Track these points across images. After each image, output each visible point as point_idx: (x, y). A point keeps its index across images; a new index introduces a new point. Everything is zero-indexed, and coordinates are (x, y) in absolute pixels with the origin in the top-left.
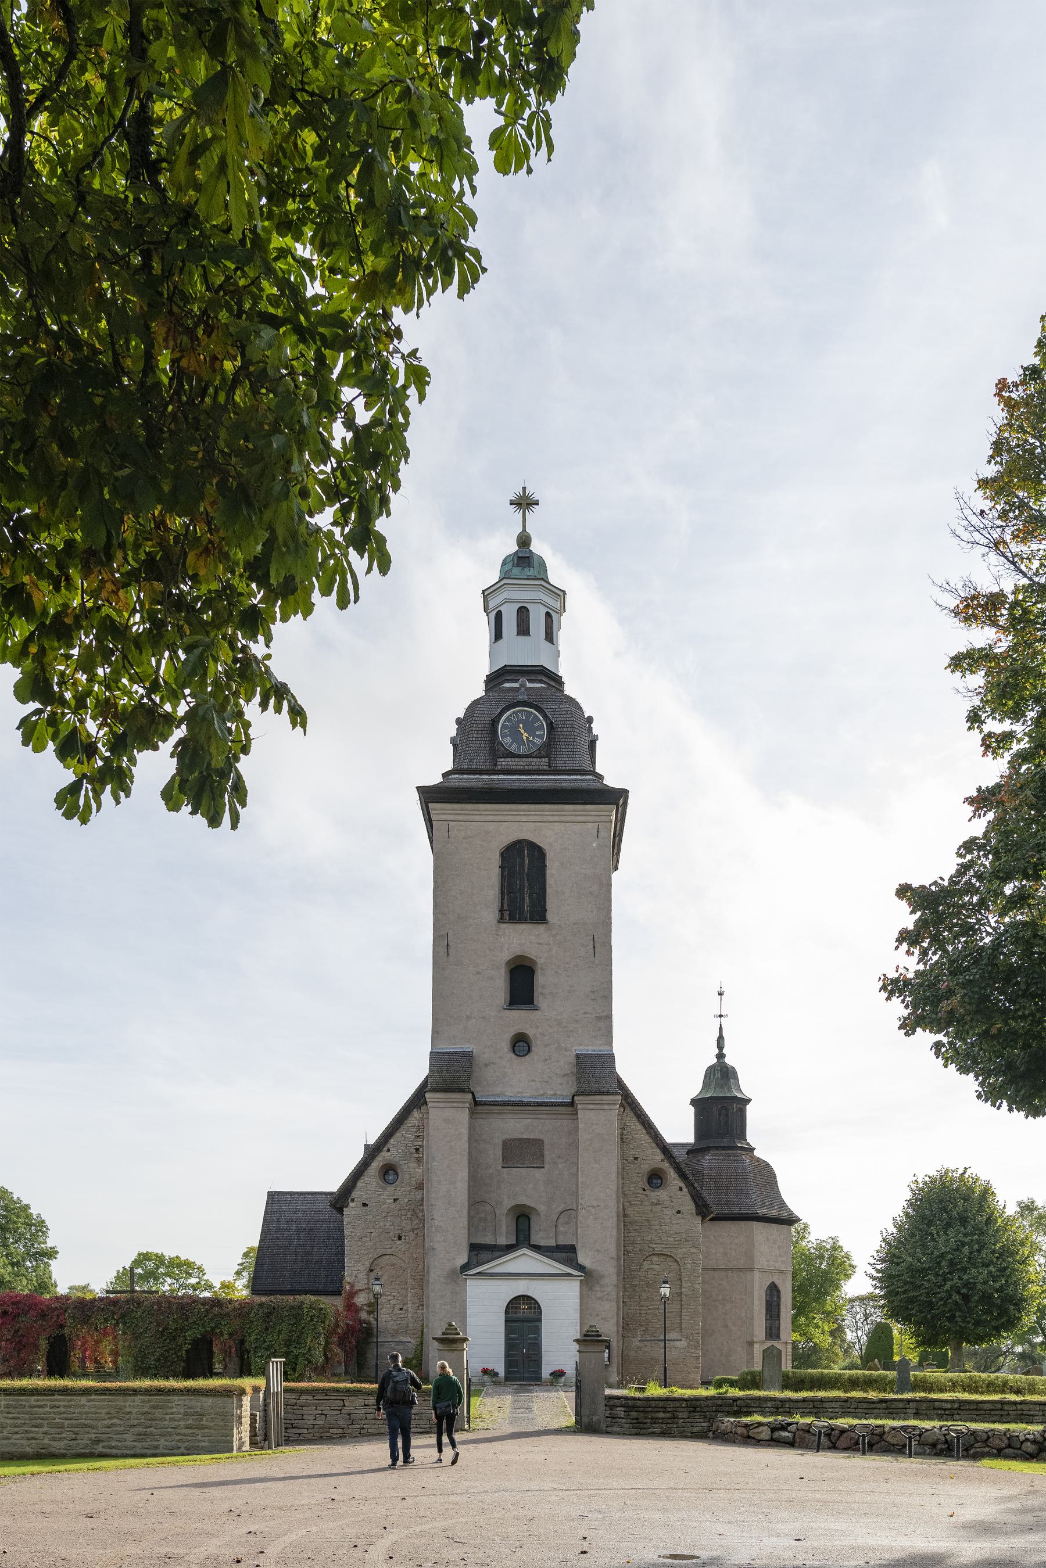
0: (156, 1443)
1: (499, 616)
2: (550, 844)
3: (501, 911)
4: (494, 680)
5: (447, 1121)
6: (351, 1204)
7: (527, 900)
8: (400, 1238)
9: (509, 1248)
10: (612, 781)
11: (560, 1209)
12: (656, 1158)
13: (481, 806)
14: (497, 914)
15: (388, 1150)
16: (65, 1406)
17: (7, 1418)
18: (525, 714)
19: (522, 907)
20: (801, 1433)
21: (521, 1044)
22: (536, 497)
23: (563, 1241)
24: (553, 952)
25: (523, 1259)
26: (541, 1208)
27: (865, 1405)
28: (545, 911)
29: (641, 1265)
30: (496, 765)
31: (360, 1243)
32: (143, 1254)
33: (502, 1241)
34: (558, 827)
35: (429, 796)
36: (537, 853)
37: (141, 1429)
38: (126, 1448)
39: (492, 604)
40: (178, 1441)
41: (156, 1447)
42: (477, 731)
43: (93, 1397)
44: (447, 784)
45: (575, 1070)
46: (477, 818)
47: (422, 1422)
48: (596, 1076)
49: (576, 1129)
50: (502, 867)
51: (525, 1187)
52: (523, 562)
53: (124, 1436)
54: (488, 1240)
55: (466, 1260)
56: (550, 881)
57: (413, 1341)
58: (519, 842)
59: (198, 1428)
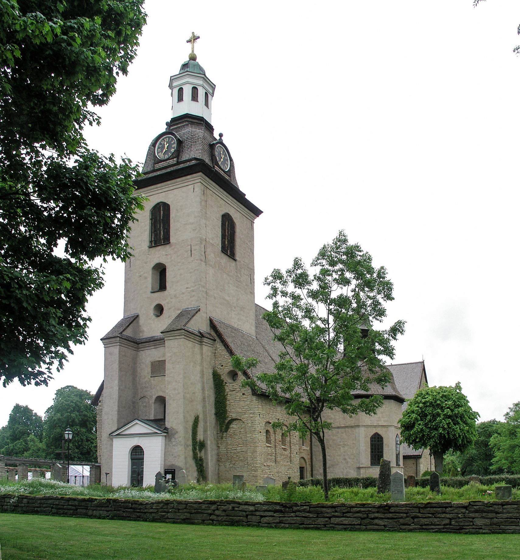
1: (181, 91)
3: (151, 242)
21: (159, 310)
24: (173, 258)
25: (137, 426)
52: (191, 66)
58: (158, 204)
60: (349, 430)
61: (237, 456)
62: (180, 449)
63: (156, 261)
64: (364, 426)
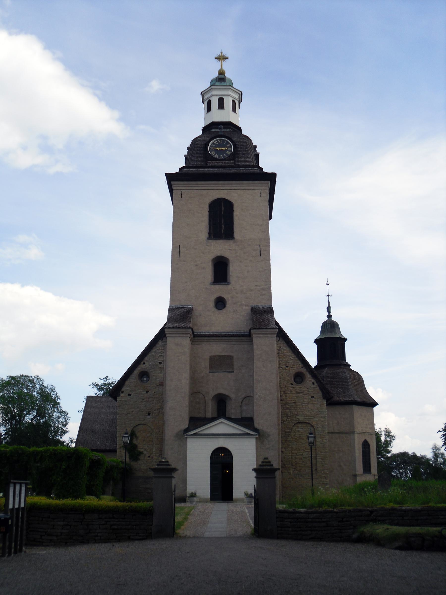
1: (209, 103)
4: (205, 129)
8: (149, 414)
10: (266, 170)
11: (243, 396)
13: (199, 182)
14: (207, 235)
15: (144, 363)
18: (222, 141)
21: (220, 303)
22: (227, 56)
23: (245, 415)
25: (221, 426)
26: (232, 396)
28: (233, 233)
29: (292, 429)
30: (207, 164)
31: (126, 417)
33: (209, 415)
35: (171, 178)
39: (205, 97)
46: (197, 188)
48: (263, 319)
49: (252, 349)
51: (222, 383)
52: (221, 79)
55: (187, 426)
61: (303, 462)
63: (218, 253)
64: (359, 433)
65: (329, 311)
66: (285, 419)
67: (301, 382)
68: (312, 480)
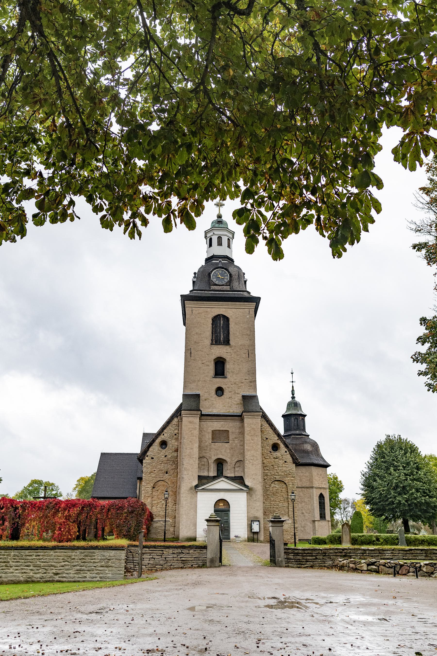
0: (85, 575)
1: (211, 239)
2: (231, 316)
3: (212, 340)
4: (208, 260)
5: (190, 422)
6: (147, 458)
7: (222, 336)
8: (167, 473)
9: (214, 478)
10: (254, 294)
11: (236, 460)
12: (275, 439)
16: (43, 555)
17: (13, 562)
19: (220, 339)
20: (382, 566)
21: (220, 391)
23: (238, 474)
26: (228, 460)
27: (402, 552)
32: (33, 481)
34: (234, 310)
35: (185, 298)
36: (226, 319)
37: (78, 568)
38: (70, 578)
40: (96, 574)
41: (85, 577)
42: (202, 277)
43: (57, 550)
44: (191, 294)
45: (242, 402)
47: (199, 562)
48: (250, 401)
50: (212, 324)
51: (222, 451)
53: (70, 571)
54: (205, 474)
56: (231, 330)
57: (171, 521)
59: (107, 567)
60: (305, 490)
62: (258, 504)
64: (317, 488)
65: (293, 394)
66: (265, 478)
67: (277, 450)
68: (295, 533)
